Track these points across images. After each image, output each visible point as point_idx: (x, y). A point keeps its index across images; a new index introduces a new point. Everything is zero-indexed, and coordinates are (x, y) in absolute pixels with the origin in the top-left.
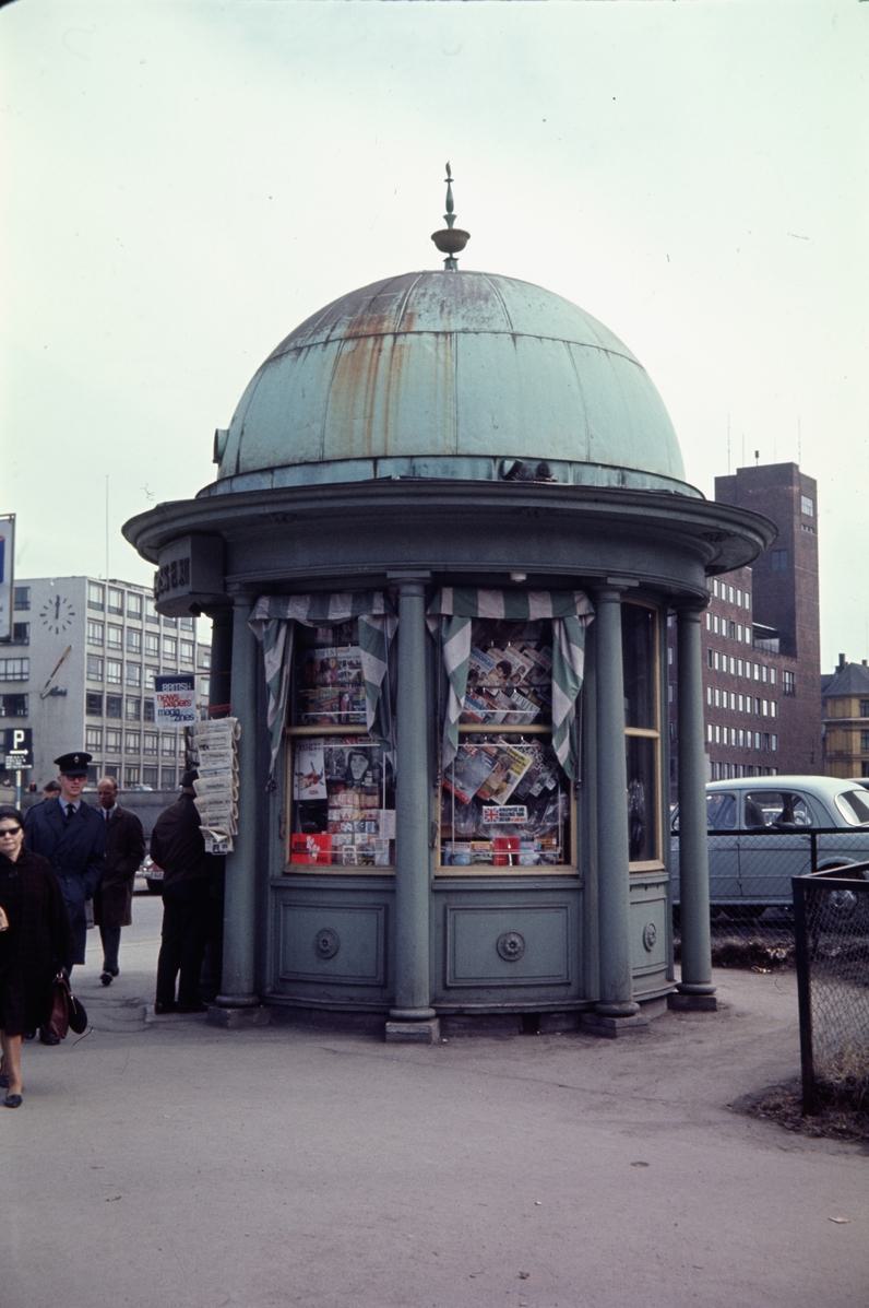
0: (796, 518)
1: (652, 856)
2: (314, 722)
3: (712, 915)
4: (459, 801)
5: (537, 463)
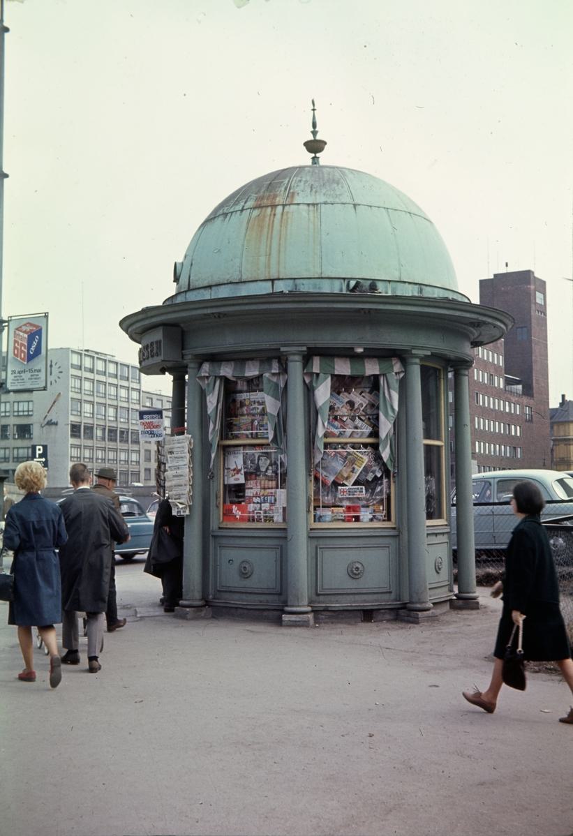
0: (533, 306)
1: (440, 517)
2: (236, 437)
3: (477, 556)
4: (324, 484)
5: (369, 282)
